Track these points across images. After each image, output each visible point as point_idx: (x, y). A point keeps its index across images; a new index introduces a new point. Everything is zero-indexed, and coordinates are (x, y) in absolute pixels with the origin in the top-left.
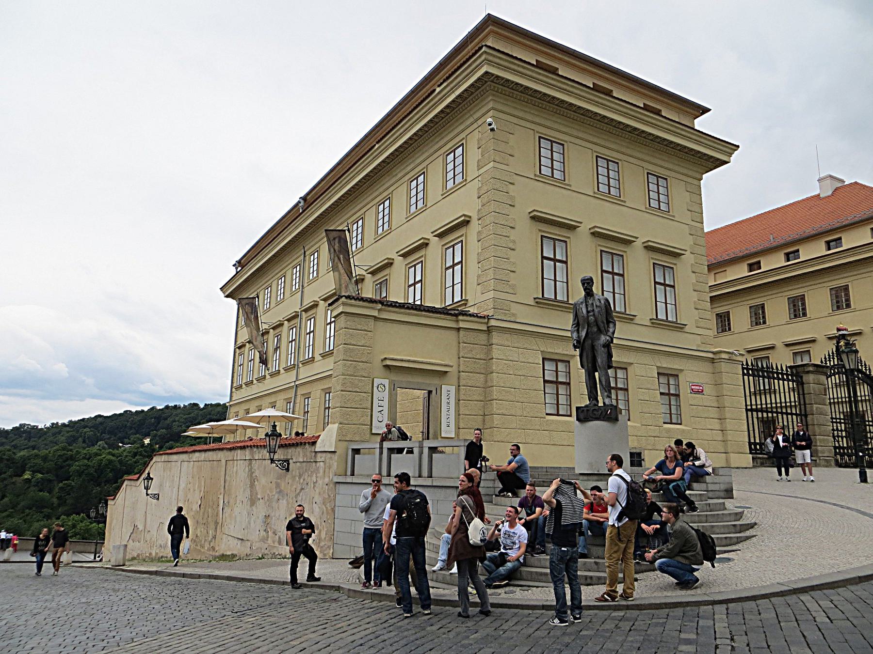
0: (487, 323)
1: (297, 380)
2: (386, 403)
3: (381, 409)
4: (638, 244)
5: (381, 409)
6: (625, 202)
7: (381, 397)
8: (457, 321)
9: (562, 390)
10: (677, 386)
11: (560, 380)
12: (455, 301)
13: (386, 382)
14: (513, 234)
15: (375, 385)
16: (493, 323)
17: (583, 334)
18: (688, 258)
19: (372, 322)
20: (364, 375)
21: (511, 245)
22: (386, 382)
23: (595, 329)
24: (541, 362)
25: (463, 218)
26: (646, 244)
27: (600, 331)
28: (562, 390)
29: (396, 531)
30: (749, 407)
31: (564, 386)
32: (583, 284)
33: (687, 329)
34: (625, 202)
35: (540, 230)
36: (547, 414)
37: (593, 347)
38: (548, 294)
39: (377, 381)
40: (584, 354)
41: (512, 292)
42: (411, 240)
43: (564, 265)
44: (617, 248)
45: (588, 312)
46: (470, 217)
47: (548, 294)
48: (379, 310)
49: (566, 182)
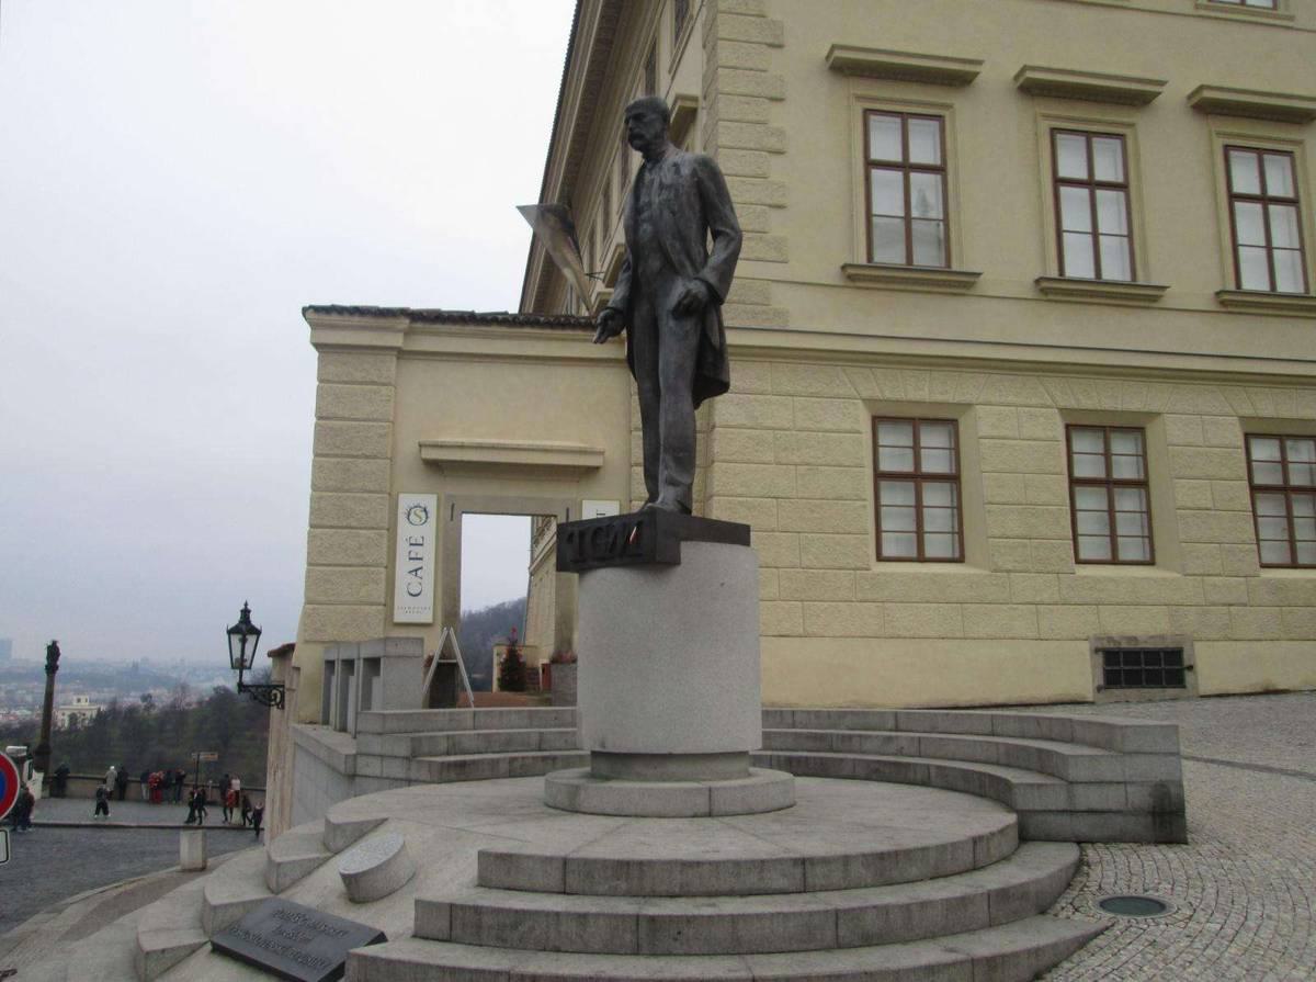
2: (429, 553)
3: (417, 564)
5: (417, 564)
6: (1291, 18)
7: (417, 532)
9: (935, 496)
10: (956, 450)
11: (927, 468)
13: (430, 501)
14: (778, 116)
15: (402, 509)
19: (391, 363)
20: (371, 487)
21: (773, 142)
22: (430, 501)
24: (1241, 442)
26: (1195, 100)
28: (935, 496)
30: (1127, 502)
31: (1133, 491)
33: (1167, 302)
34: (1291, 18)
36: (1264, 566)
38: (1249, 283)
39: (406, 501)
41: (773, 255)
43: (1121, 195)
47: (1255, 280)
48: (408, 333)
49: (1281, 11)
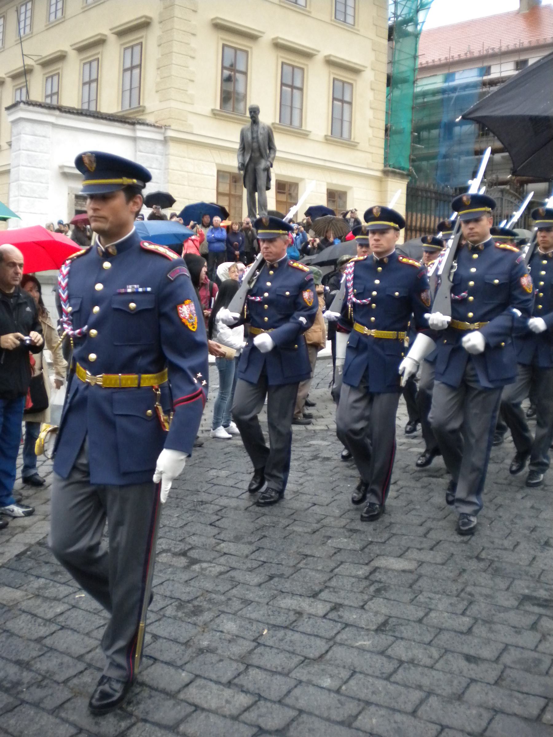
0: (164, 134)
1: (541, 616)
4: (319, 58)
8: (134, 130)
12: (133, 107)
16: (170, 133)
17: (247, 159)
18: (368, 76)
23: (258, 154)
25: (143, 20)
27: (262, 156)
29: (120, 177)
32: (250, 112)
34: (310, 12)
35: (222, 39)
37: (255, 171)
40: (247, 176)
42: (87, 34)
44: (298, 61)
45: (253, 138)
46: (151, 18)
